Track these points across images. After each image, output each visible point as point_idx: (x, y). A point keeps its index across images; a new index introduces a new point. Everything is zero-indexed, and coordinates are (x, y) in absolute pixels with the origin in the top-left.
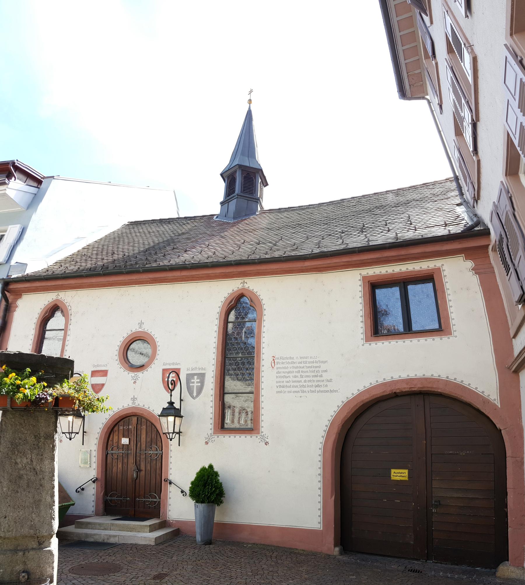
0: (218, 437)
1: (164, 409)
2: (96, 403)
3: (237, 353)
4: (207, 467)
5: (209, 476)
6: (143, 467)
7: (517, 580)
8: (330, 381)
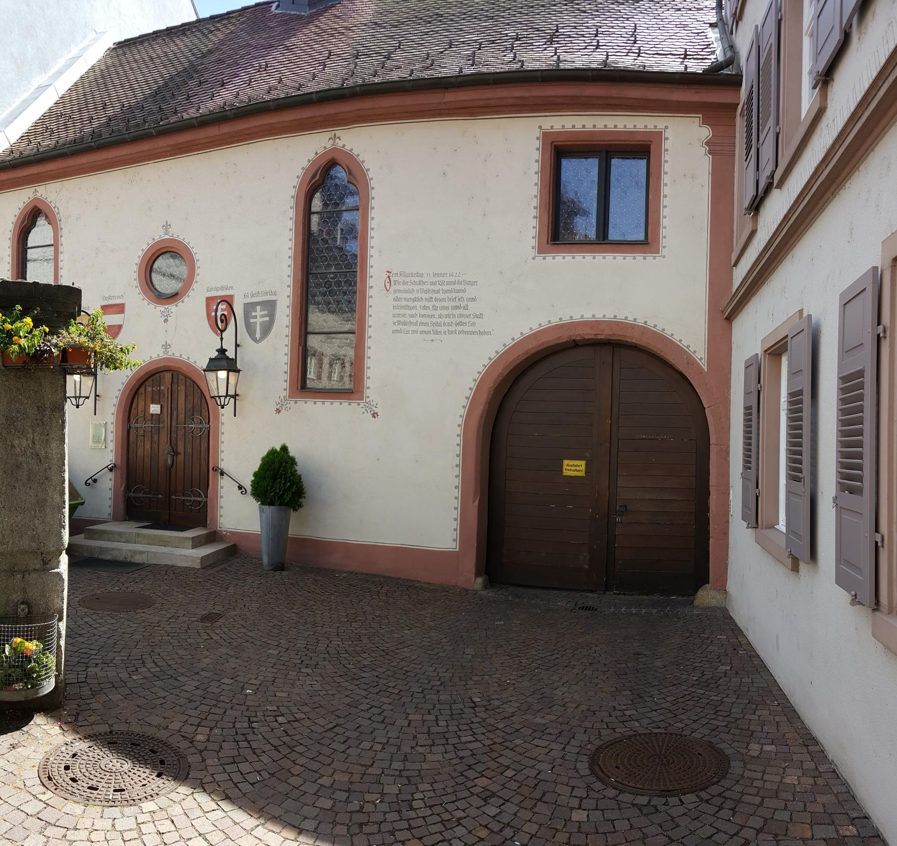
0: (296, 403)
1: (211, 359)
2: (120, 355)
3: (328, 267)
4: (278, 449)
5: (281, 464)
6: (181, 449)
7: (718, 608)
8: (480, 316)
